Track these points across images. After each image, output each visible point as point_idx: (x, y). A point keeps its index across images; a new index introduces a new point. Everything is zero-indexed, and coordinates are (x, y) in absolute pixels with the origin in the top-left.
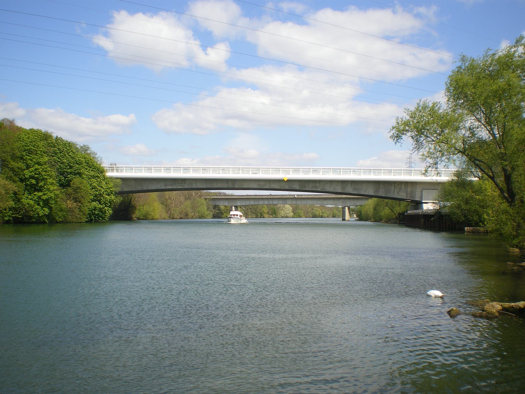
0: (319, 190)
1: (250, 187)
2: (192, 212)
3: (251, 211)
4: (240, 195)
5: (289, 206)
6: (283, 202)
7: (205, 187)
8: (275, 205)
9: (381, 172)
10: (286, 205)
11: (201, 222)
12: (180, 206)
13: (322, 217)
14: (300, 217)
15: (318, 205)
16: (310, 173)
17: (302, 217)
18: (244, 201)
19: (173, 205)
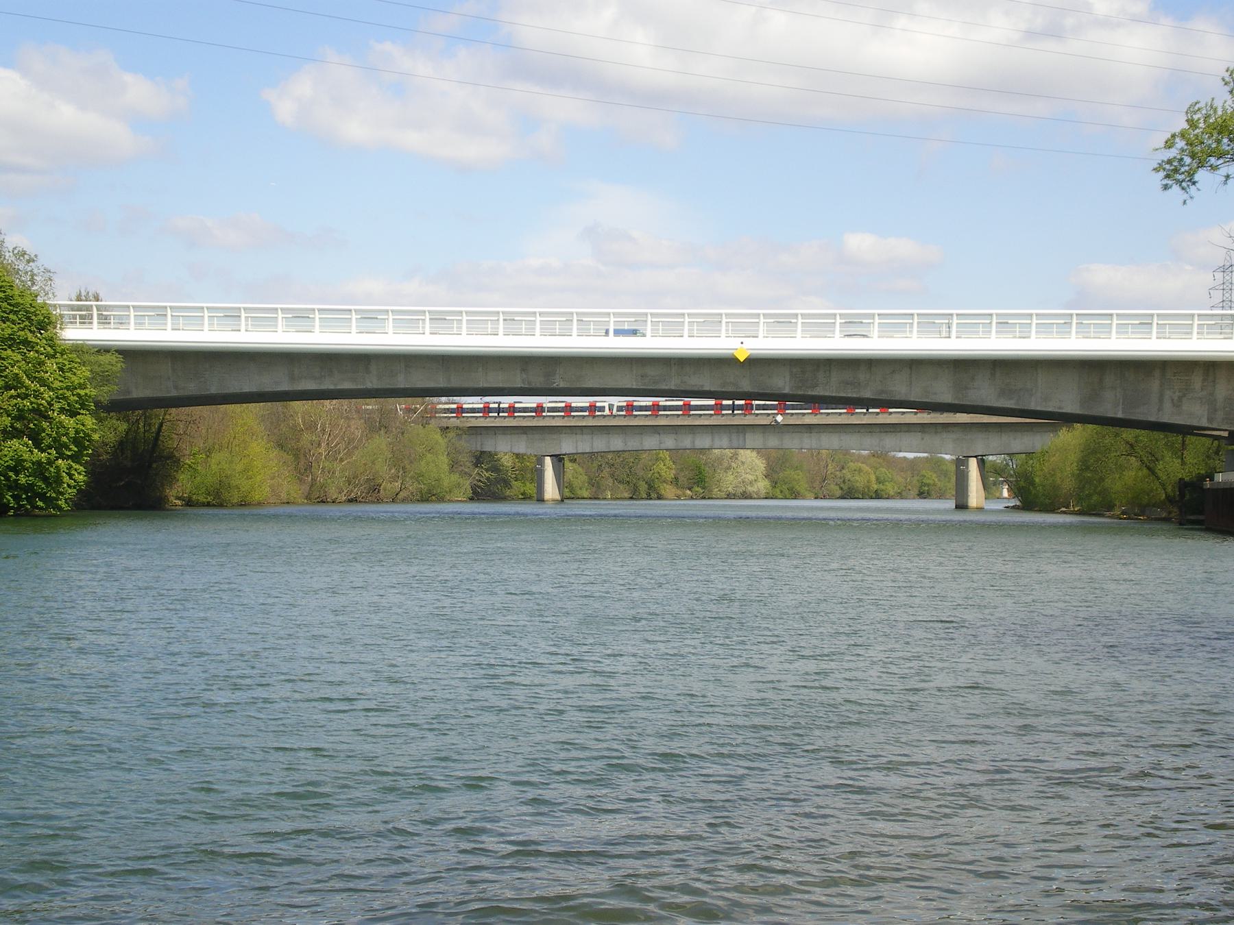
2: (394, 478)
3: (612, 475)
5: (754, 454)
7: (442, 386)
9: (646, 321)
10: (742, 451)
12: (349, 454)
13: (878, 496)
14: (795, 495)
16: (833, 332)
17: (804, 498)
18: (587, 437)
19: (322, 450)
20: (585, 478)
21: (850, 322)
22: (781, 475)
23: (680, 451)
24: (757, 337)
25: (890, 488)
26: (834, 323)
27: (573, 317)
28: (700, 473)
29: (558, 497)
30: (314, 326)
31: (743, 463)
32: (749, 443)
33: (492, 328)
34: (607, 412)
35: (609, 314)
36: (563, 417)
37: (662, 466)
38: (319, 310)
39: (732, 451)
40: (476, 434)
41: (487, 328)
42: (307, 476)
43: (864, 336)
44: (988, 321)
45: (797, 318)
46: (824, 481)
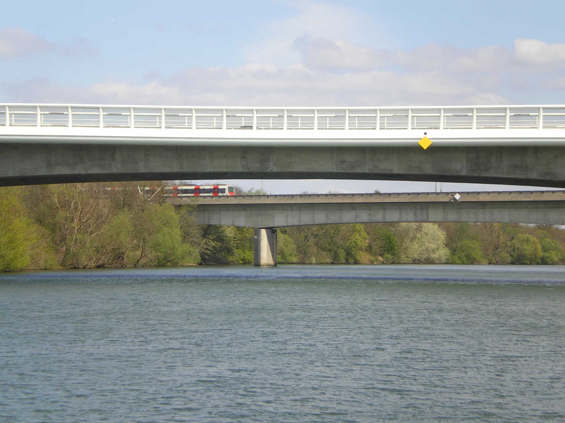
0: (534, 176)
1: (315, 168)
2: (136, 248)
3: (317, 244)
4: (284, 196)
5: (436, 226)
6: (416, 215)
7: (175, 171)
8: (392, 224)
9: (344, 116)
10: (425, 224)
11: (170, 280)
12: (98, 228)
13: (543, 262)
14: (472, 261)
15: (532, 225)
16: (504, 123)
17: (479, 263)
18: (295, 213)
19: (75, 224)
20: (293, 246)
21: (518, 115)
22: (459, 244)
23: (373, 224)
24: (222, 128)
25: (554, 255)
26: (505, 116)
27: (284, 113)
28: (390, 242)
29: (271, 262)
30: (67, 121)
31: (426, 234)
32: (431, 218)
33: (217, 123)
34: (227, 193)
35: (313, 111)
36: (212, 197)
37: (358, 236)
38: (72, 108)
39: (417, 224)
40: (204, 210)
41: (213, 123)
42: (62, 247)
43: (65, 126)
44: (220, 115)
45: (473, 113)
46: (496, 249)
